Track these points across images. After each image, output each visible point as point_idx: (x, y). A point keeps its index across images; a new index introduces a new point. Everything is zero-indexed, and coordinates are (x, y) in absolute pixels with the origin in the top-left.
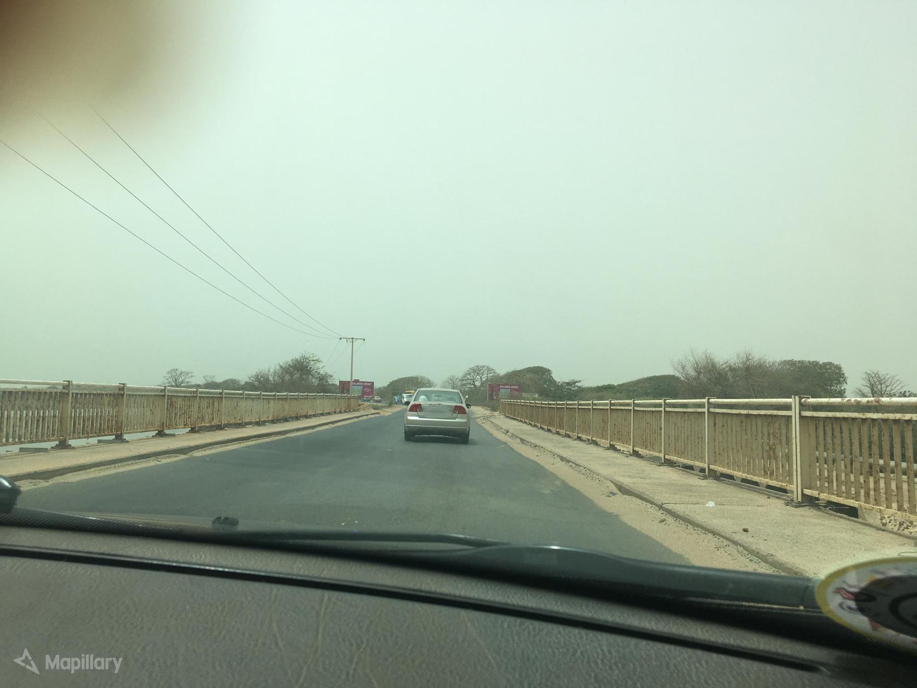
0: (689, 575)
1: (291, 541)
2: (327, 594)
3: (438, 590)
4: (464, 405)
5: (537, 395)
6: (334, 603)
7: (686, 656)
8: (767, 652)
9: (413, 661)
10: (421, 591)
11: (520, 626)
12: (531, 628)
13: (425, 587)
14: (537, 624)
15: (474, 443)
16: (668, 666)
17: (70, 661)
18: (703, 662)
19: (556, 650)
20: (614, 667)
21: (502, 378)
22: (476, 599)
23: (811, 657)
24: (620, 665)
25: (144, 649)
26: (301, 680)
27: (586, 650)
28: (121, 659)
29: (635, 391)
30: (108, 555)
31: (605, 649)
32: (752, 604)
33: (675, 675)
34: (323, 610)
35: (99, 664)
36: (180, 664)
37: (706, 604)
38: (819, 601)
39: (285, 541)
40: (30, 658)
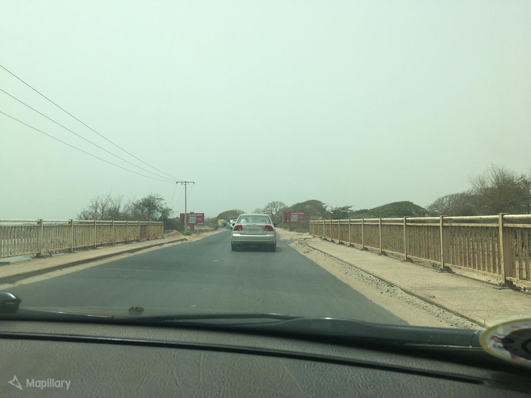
0: (407, 331)
2: (203, 353)
4: (272, 225)
5: (305, 216)
6: (208, 359)
7: (408, 379)
9: (255, 390)
10: (255, 348)
12: (320, 367)
13: (257, 346)
15: (280, 250)
17: (41, 382)
20: (369, 388)
21: (290, 208)
22: (287, 351)
23: (479, 376)
25: (101, 390)
28: (70, 381)
29: (383, 213)
30: (78, 335)
31: (363, 377)
34: (201, 362)
35: (57, 384)
38: (481, 342)
40: (17, 381)
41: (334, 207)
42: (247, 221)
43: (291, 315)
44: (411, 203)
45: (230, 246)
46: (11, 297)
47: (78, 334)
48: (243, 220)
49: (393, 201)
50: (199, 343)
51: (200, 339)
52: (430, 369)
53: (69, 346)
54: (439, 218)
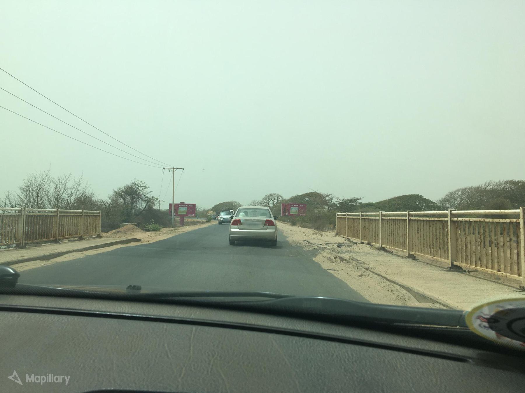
1: (176, 298)
2: (194, 328)
4: (272, 219)
5: (312, 210)
10: (246, 324)
12: (308, 343)
14: (311, 340)
15: (280, 247)
16: (384, 362)
18: (404, 359)
20: (355, 363)
21: (288, 200)
22: (277, 328)
23: (464, 354)
24: (358, 362)
26: (182, 376)
27: (339, 354)
28: (69, 377)
31: (349, 353)
32: (432, 326)
33: (389, 366)
35: (57, 379)
36: (114, 369)
37: (405, 326)
38: (468, 323)
40: (17, 376)
41: (341, 198)
43: (283, 294)
44: (421, 197)
45: (227, 239)
46: (9, 272)
47: (74, 308)
48: (242, 214)
49: (401, 194)
50: (192, 319)
52: (417, 347)
54: (447, 212)
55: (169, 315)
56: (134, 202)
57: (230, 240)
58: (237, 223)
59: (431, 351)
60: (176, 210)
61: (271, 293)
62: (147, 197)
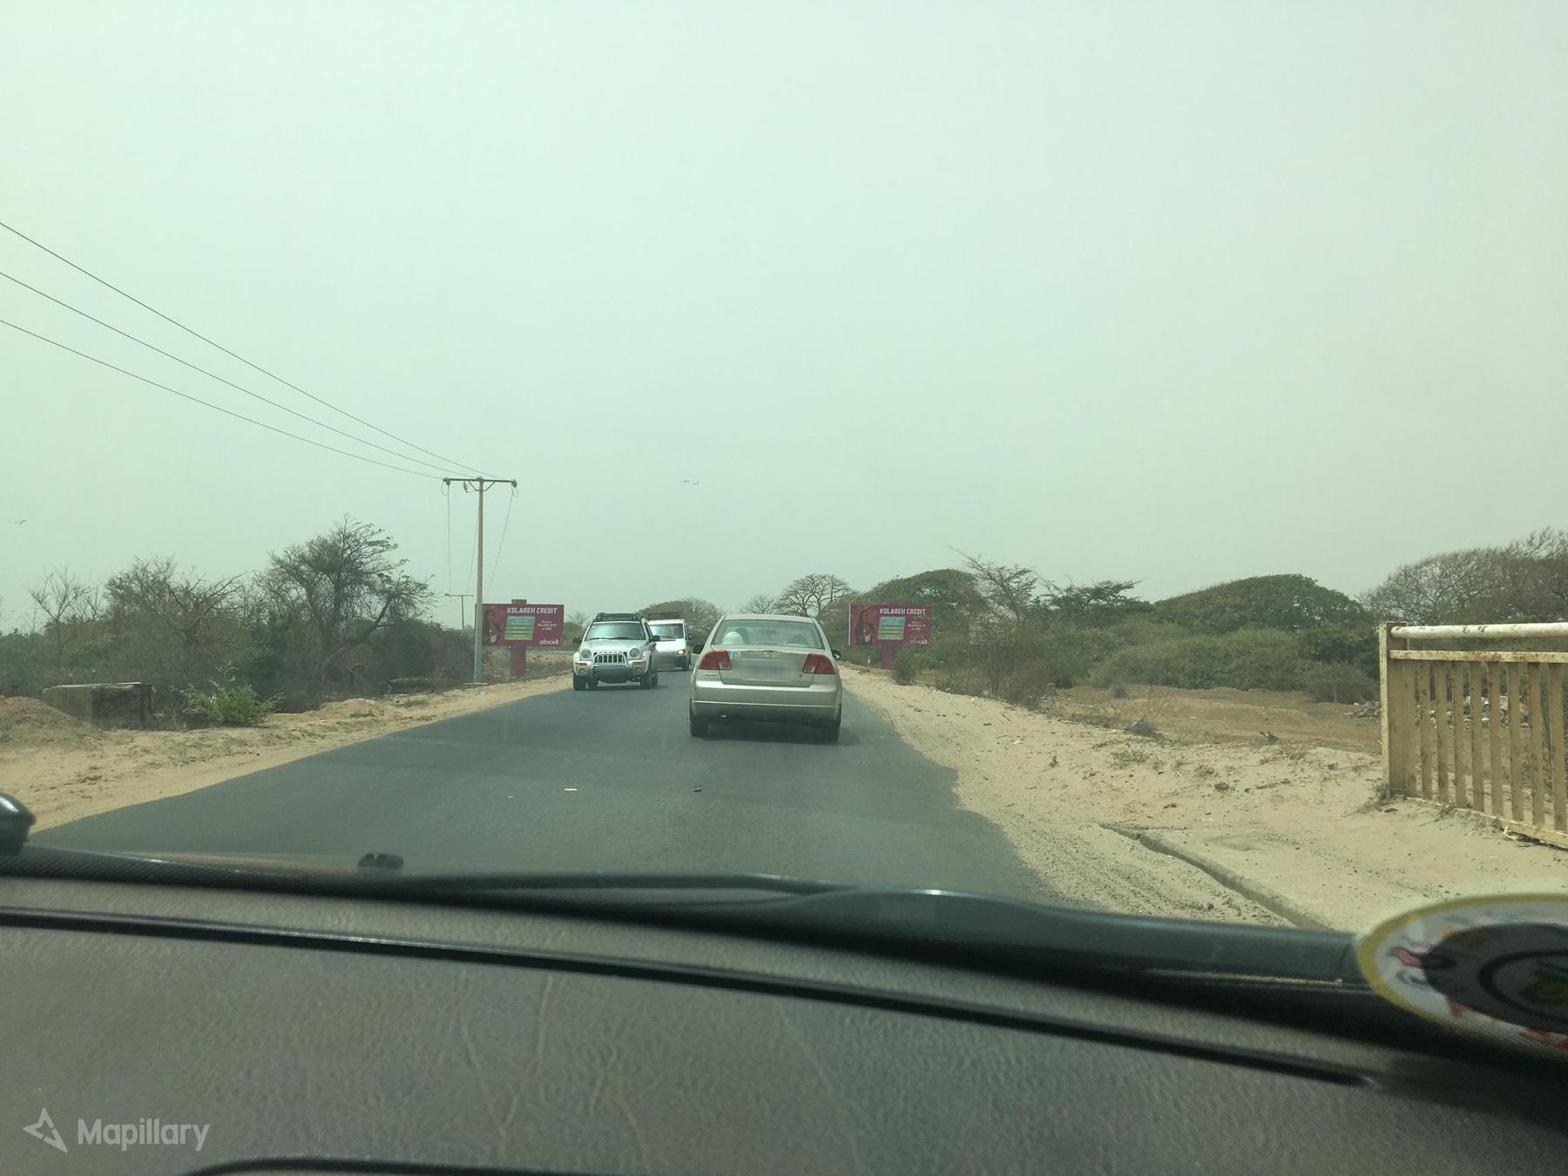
1: (490, 892)
2: (551, 977)
3: (736, 967)
4: (827, 653)
5: (946, 626)
8: (1290, 1057)
10: (708, 968)
11: (871, 1021)
12: (889, 1025)
14: (900, 1018)
15: (853, 740)
16: (1114, 1081)
17: (120, 1130)
18: (1173, 1074)
19: (930, 1060)
20: (1025, 1084)
21: (867, 596)
23: (1352, 1062)
24: (1035, 1082)
26: (510, 1118)
28: (206, 1127)
31: (1011, 1056)
34: (544, 1003)
38: (1365, 971)
39: (480, 891)
40: (51, 1125)
42: (746, 639)
44: (1309, 583)
48: (731, 635)
51: (548, 941)
53: (165, 947)
55: (479, 940)
56: (346, 596)
57: (693, 717)
58: (718, 661)
59: (1257, 1052)
60: (500, 628)
61: (787, 878)
62: (389, 580)
